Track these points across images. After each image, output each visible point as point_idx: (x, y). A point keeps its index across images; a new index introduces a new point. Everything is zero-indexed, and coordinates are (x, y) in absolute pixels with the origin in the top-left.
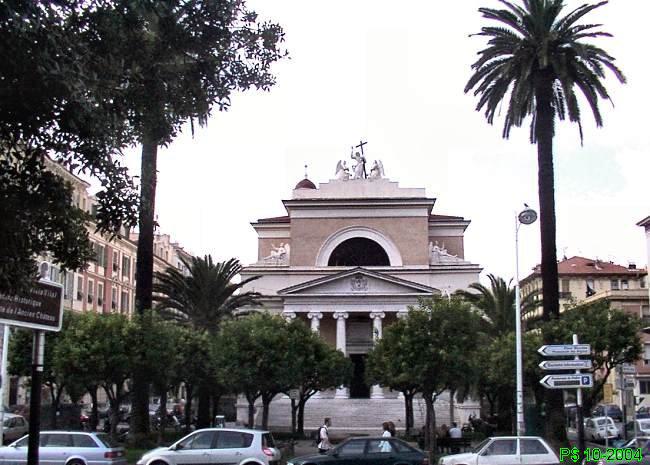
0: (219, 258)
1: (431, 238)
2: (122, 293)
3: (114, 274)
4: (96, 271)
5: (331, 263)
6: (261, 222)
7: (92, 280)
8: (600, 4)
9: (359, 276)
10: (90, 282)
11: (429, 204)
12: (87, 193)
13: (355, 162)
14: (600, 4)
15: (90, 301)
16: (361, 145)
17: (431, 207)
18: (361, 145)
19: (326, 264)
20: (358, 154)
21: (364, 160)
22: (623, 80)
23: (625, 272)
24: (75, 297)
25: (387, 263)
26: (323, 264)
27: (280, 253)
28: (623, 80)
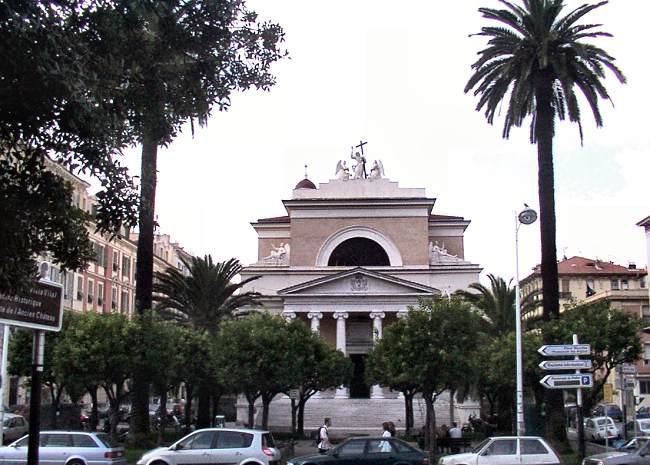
0: (219, 258)
1: (431, 238)
2: (122, 293)
3: (114, 274)
4: (96, 271)
5: (331, 263)
6: (261, 222)
7: (92, 280)
8: (600, 4)
9: (359, 276)
10: (90, 282)
11: (429, 203)
12: (87, 193)
13: (355, 162)
14: (600, 4)
15: (90, 301)
16: (361, 145)
17: (431, 207)
18: (361, 145)
19: (326, 264)
20: (358, 154)
21: (364, 160)
22: (623, 80)
23: (625, 272)
24: (75, 297)
25: (387, 263)
26: (323, 264)
27: (280, 253)
28: (623, 80)
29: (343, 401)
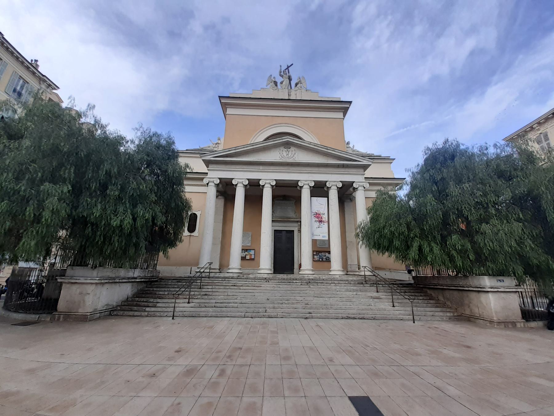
21: (290, 79)
29: (266, 276)
